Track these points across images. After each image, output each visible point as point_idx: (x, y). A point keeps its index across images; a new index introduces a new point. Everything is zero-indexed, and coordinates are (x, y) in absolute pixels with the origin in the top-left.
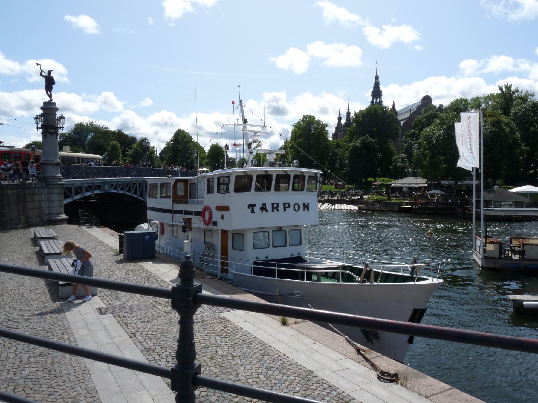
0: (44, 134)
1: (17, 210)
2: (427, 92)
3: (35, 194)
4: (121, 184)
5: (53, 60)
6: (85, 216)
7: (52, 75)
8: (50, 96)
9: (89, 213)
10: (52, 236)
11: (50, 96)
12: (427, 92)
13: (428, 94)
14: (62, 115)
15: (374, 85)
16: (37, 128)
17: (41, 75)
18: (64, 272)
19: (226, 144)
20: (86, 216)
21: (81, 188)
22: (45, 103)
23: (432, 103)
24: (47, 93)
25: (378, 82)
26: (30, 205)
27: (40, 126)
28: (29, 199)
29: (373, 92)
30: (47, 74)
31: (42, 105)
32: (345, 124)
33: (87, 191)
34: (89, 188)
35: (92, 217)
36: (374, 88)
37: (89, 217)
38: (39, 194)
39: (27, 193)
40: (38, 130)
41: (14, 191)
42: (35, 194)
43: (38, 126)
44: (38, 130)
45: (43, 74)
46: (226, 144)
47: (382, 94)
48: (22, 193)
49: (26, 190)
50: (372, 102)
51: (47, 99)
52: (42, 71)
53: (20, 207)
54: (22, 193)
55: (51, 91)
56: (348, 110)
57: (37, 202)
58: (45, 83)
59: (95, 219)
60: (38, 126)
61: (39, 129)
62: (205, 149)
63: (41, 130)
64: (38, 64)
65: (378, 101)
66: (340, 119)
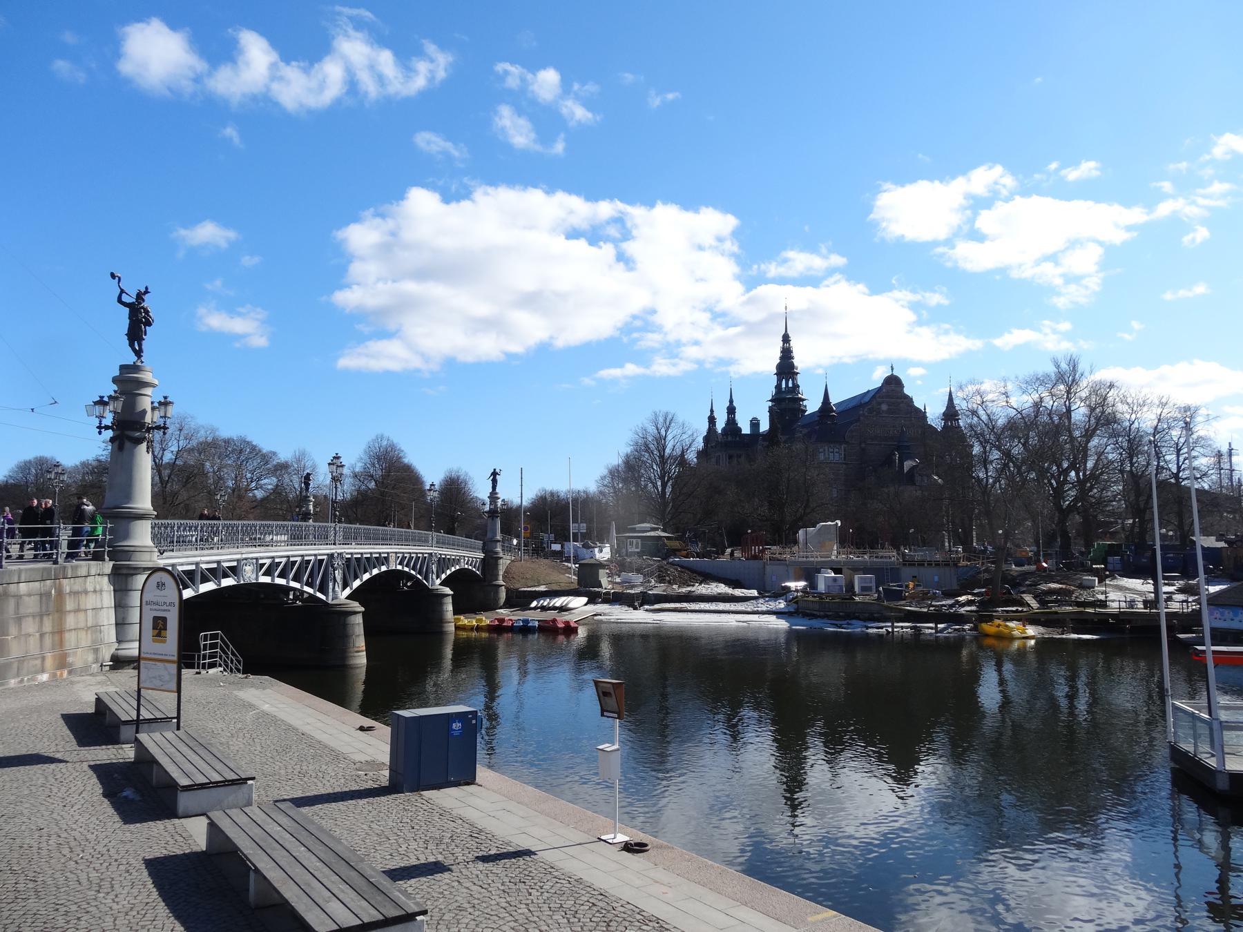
0: (117, 443)
1: (38, 635)
2: (892, 369)
3: (86, 592)
4: (281, 562)
5: (920, 181)
6: (213, 646)
7: (148, 303)
8: (138, 353)
9: (222, 640)
10: (201, 780)
11: (138, 353)
12: (892, 369)
13: (895, 373)
14: (165, 398)
15: (781, 352)
16: (100, 427)
17: (120, 301)
18: (40, 662)
19: (495, 470)
20: (213, 646)
21: (190, 574)
22: (123, 368)
23: (902, 390)
24: (132, 345)
25: (790, 348)
26: (70, 621)
27: (108, 421)
28: (70, 605)
29: (779, 367)
30: (134, 301)
31: (117, 373)
32: (724, 429)
33: (205, 580)
34: (216, 573)
35: (228, 647)
36: (781, 358)
37: (222, 649)
38: (95, 591)
39: (67, 589)
40: (100, 433)
41: (36, 586)
42: (86, 592)
43: (100, 424)
44: (100, 433)
45: (125, 298)
46: (495, 470)
47: (126, 337)
48: (53, 591)
49: (65, 582)
50: (778, 387)
51: (130, 359)
52: (122, 291)
53: (48, 625)
54: (53, 591)
55: (140, 340)
56: (731, 401)
57: (90, 613)
58: (128, 321)
59: (233, 654)
60: (100, 424)
61: (103, 430)
62: (953, 588)
63: (109, 434)
64: (113, 276)
65: (790, 385)
66: (712, 420)
